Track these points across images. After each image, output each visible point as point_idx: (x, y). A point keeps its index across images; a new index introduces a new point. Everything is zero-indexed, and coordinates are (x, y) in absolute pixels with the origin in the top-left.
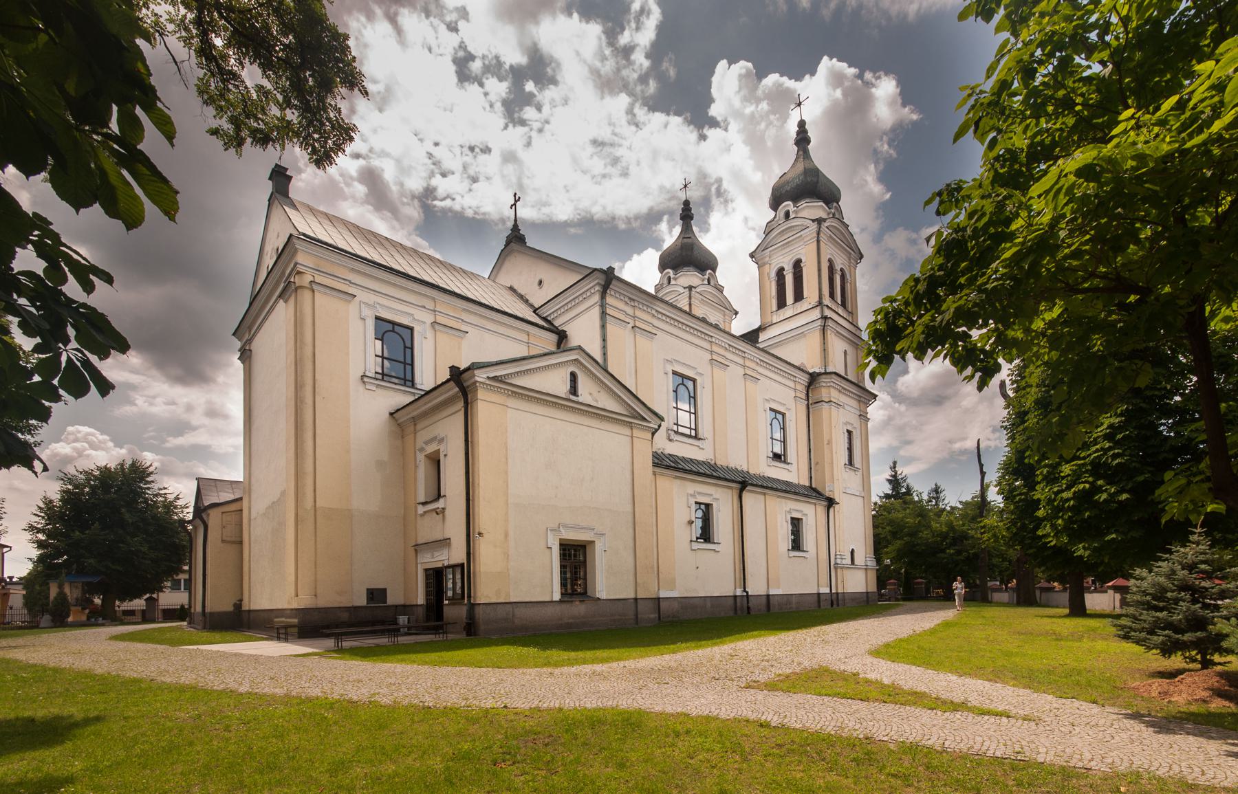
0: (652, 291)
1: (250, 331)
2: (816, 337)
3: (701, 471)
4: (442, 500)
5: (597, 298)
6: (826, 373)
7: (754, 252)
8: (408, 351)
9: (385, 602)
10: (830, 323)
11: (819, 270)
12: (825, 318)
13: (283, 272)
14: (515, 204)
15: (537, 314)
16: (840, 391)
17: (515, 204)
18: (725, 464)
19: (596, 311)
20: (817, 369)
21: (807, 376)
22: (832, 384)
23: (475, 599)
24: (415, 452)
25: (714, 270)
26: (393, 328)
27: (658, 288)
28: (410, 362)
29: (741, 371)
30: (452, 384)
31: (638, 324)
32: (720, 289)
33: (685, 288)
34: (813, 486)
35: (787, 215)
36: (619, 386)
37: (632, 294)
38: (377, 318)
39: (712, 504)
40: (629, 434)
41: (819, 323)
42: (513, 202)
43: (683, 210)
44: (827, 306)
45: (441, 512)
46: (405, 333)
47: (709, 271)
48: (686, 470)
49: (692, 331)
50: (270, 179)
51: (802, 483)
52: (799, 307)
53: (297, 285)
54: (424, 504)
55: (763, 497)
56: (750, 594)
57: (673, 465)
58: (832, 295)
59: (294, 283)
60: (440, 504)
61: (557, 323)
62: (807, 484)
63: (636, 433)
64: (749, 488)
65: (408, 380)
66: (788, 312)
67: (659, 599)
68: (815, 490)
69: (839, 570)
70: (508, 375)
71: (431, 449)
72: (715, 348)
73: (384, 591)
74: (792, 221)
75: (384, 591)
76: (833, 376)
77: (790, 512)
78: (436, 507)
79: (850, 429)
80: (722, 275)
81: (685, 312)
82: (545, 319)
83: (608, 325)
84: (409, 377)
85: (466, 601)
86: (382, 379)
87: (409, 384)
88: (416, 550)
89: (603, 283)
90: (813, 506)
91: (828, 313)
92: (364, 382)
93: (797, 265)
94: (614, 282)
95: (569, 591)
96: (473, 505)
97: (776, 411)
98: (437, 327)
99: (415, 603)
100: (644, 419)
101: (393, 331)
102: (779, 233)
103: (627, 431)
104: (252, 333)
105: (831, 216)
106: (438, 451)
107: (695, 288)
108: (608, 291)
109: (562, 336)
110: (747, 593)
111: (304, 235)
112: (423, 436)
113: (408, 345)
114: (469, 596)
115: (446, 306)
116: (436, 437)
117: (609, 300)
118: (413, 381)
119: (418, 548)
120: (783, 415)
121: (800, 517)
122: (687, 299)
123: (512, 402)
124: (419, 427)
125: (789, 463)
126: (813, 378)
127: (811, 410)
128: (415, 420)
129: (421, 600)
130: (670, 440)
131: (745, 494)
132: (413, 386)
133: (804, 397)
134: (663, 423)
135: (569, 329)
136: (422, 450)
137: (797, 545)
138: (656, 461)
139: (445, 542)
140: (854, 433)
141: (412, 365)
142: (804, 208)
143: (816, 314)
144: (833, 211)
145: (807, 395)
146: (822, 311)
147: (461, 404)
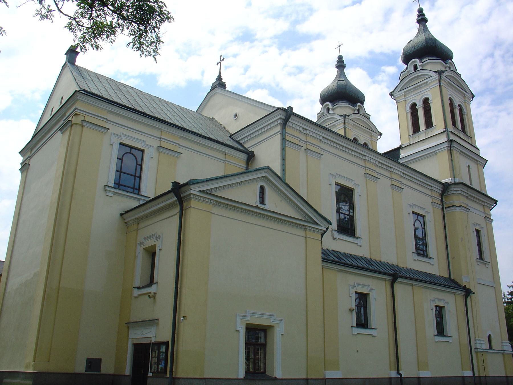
0: (315, 120)
1: (31, 151)
2: (445, 156)
3: (360, 265)
4: (154, 286)
5: (279, 128)
6: (455, 184)
7: (392, 92)
8: (139, 167)
9: (100, 372)
10: (454, 145)
11: (443, 106)
12: (451, 141)
13: (64, 114)
14: (220, 63)
15: (232, 138)
16: (467, 198)
17: (220, 63)
18: (378, 259)
19: (278, 138)
20: (447, 180)
21: (441, 186)
22: (460, 192)
23: (176, 375)
24: (136, 245)
25: (362, 102)
26: (131, 151)
27: (320, 116)
28: (139, 175)
29: (363, 171)
30: (172, 194)
31: (309, 147)
32: (367, 117)
33: (340, 116)
34: (452, 277)
35: (416, 67)
36: (302, 202)
37: (305, 125)
38: (121, 144)
39: (369, 294)
40: (304, 235)
41: (446, 145)
42: (219, 61)
43: (338, 62)
44: (451, 132)
45: (153, 296)
46: (138, 154)
47: (359, 104)
48: (348, 264)
49: (350, 152)
50: (66, 54)
51: (442, 275)
52: (430, 132)
53: (73, 122)
54: (139, 288)
55: (411, 287)
56: (403, 376)
57: (336, 259)
58: (454, 124)
59: (71, 121)
60: (152, 289)
61: (247, 146)
62: (446, 276)
63: (309, 234)
64: (399, 280)
65: (136, 189)
66: (422, 136)
67: (326, 379)
68: (453, 281)
69: (479, 355)
70: (214, 188)
71: (149, 243)
72: (368, 165)
73: (99, 361)
74: (420, 71)
75: (99, 361)
76: (461, 186)
77: (433, 301)
78: (148, 291)
79: (478, 228)
80: (368, 106)
81: (341, 136)
82: (238, 142)
83: (286, 148)
84: (137, 186)
85: (168, 375)
86: (118, 189)
87: (136, 191)
88: (128, 328)
89: (284, 118)
90: (453, 296)
91: (452, 137)
92: (106, 190)
93: (426, 102)
94: (292, 117)
95: (251, 370)
96: (180, 292)
97: (418, 214)
98: (161, 149)
99: (122, 373)
100: (316, 223)
101: (130, 153)
102: (410, 80)
103: (302, 233)
104: (32, 153)
105: (448, 69)
106: (154, 246)
107: (348, 116)
108: (287, 124)
109: (251, 156)
110: (401, 375)
111: (84, 90)
112: (144, 233)
113: (139, 163)
114: (171, 371)
115: (168, 133)
116: (154, 235)
117: (288, 130)
118: (139, 190)
119: (130, 325)
120: (423, 217)
121: (443, 305)
122: (343, 125)
123: (216, 210)
124: (141, 225)
125: (430, 258)
126: (446, 187)
127: (445, 213)
128: (138, 220)
129: (128, 371)
130: (334, 239)
131: (397, 286)
132: (139, 194)
133: (439, 202)
134: (330, 226)
135: (257, 151)
136: (141, 244)
137: (441, 331)
138: (324, 257)
139: (154, 322)
140: (482, 232)
141: (140, 177)
142: (428, 63)
143: (443, 139)
144: (449, 65)
145: (442, 201)
146: (448, 137)
147: (178, 209)
